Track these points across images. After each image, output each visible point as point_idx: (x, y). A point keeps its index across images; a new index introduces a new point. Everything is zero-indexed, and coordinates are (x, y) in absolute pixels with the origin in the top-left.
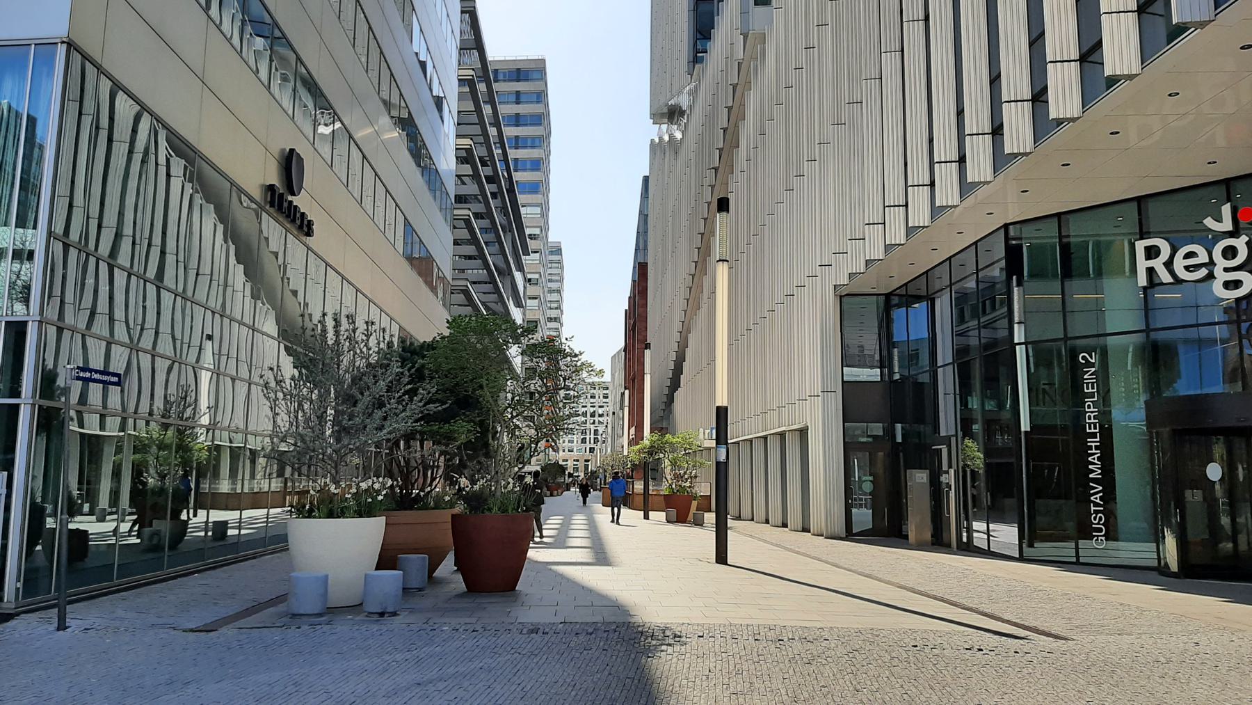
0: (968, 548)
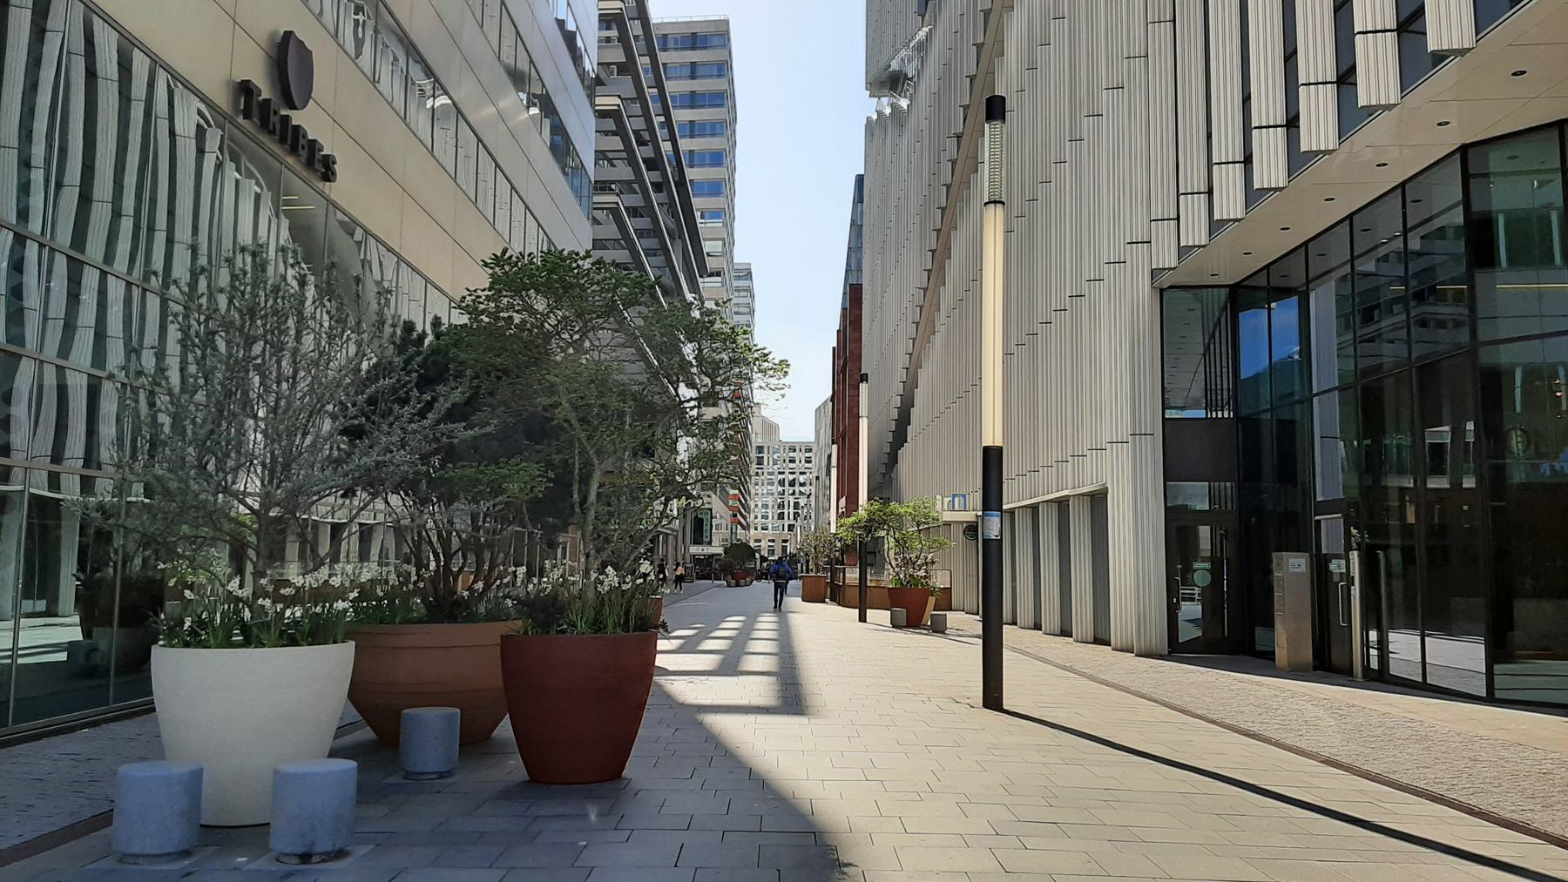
0: (1381, 678)
